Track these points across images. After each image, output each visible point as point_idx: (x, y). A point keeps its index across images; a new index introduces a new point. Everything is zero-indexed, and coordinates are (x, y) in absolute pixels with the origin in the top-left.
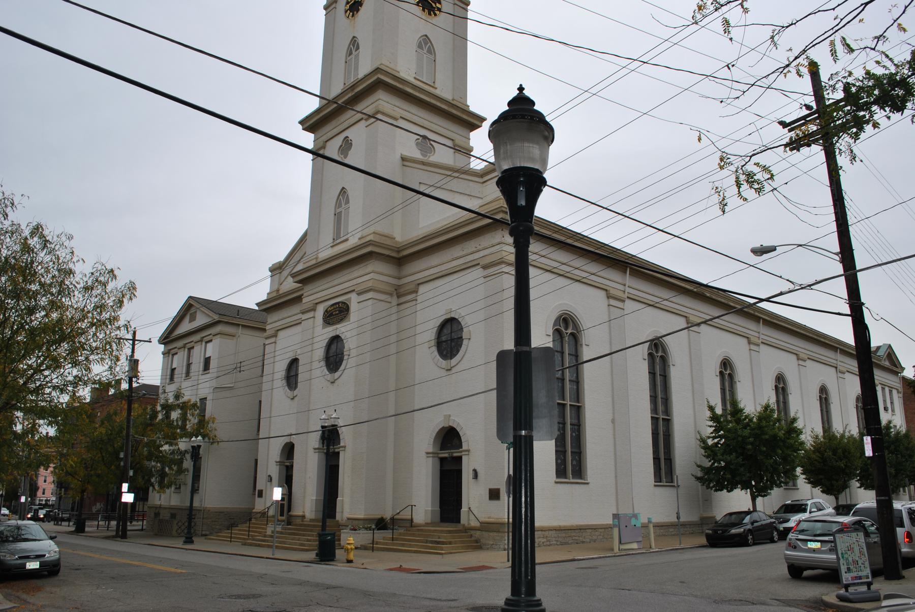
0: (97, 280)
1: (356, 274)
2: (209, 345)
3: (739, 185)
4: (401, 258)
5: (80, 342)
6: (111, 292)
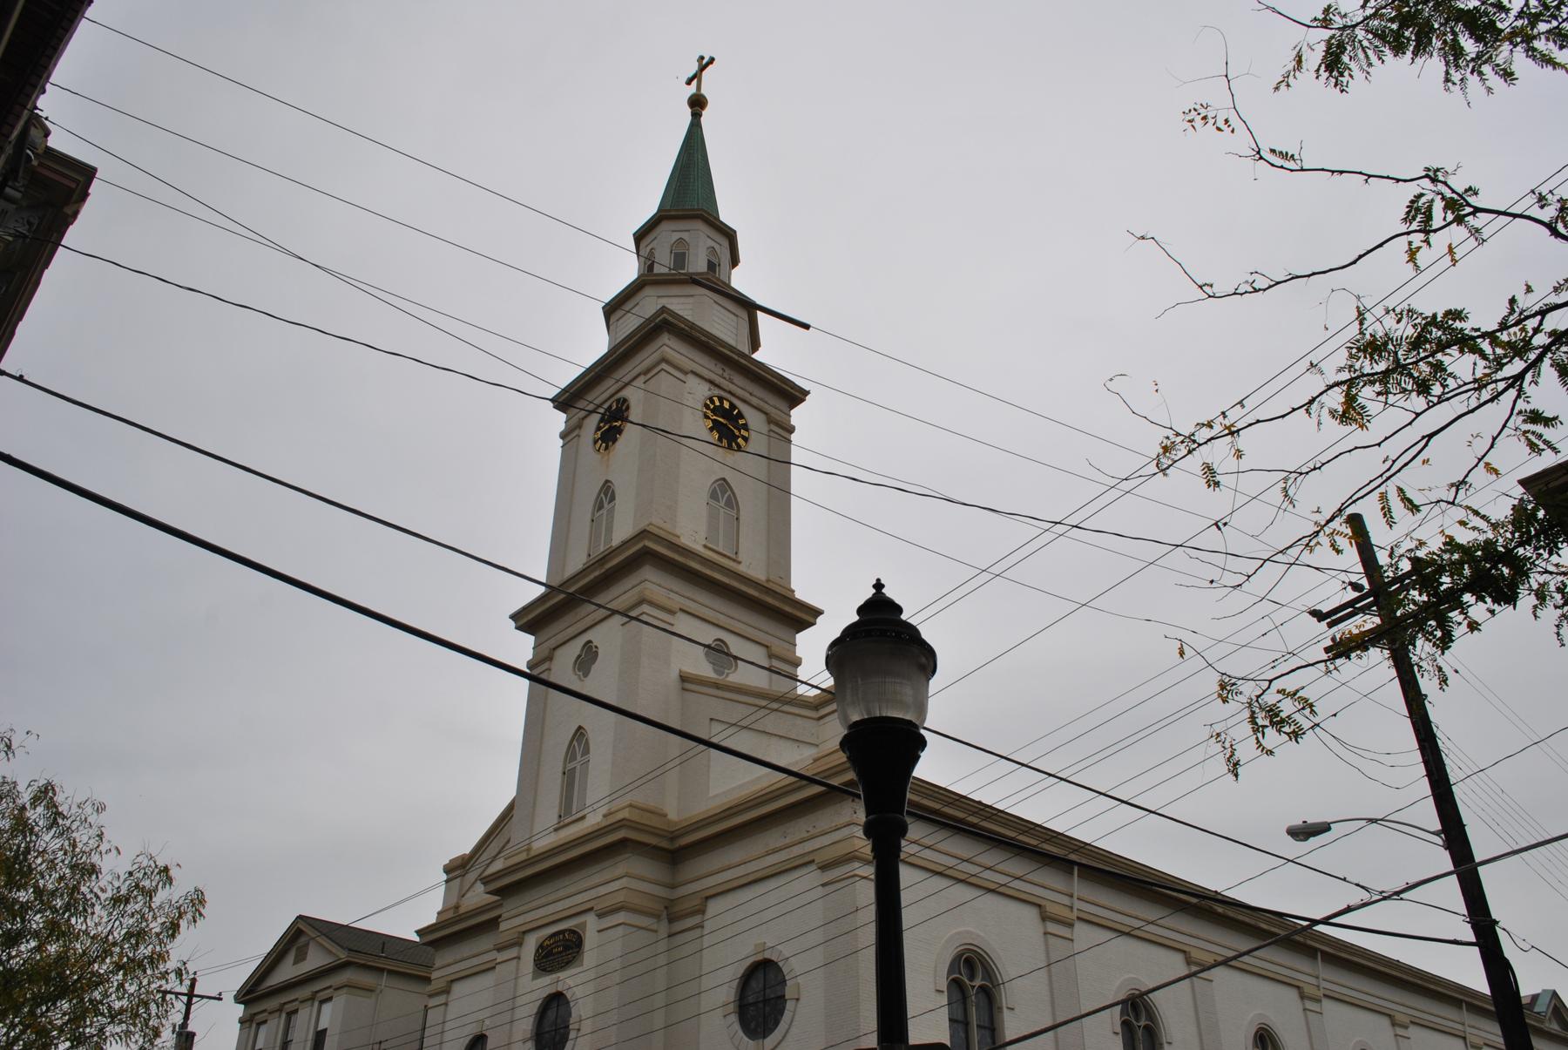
0: (137, 886)
1: (596, 879)
2: (327, 1008)
3: (1257, 728)
4: (676, 849)
5: (91, 1001)
6: (160, 907)
